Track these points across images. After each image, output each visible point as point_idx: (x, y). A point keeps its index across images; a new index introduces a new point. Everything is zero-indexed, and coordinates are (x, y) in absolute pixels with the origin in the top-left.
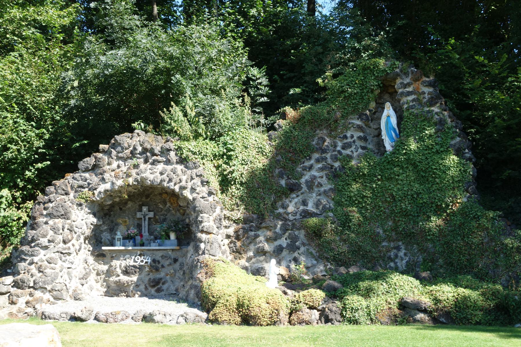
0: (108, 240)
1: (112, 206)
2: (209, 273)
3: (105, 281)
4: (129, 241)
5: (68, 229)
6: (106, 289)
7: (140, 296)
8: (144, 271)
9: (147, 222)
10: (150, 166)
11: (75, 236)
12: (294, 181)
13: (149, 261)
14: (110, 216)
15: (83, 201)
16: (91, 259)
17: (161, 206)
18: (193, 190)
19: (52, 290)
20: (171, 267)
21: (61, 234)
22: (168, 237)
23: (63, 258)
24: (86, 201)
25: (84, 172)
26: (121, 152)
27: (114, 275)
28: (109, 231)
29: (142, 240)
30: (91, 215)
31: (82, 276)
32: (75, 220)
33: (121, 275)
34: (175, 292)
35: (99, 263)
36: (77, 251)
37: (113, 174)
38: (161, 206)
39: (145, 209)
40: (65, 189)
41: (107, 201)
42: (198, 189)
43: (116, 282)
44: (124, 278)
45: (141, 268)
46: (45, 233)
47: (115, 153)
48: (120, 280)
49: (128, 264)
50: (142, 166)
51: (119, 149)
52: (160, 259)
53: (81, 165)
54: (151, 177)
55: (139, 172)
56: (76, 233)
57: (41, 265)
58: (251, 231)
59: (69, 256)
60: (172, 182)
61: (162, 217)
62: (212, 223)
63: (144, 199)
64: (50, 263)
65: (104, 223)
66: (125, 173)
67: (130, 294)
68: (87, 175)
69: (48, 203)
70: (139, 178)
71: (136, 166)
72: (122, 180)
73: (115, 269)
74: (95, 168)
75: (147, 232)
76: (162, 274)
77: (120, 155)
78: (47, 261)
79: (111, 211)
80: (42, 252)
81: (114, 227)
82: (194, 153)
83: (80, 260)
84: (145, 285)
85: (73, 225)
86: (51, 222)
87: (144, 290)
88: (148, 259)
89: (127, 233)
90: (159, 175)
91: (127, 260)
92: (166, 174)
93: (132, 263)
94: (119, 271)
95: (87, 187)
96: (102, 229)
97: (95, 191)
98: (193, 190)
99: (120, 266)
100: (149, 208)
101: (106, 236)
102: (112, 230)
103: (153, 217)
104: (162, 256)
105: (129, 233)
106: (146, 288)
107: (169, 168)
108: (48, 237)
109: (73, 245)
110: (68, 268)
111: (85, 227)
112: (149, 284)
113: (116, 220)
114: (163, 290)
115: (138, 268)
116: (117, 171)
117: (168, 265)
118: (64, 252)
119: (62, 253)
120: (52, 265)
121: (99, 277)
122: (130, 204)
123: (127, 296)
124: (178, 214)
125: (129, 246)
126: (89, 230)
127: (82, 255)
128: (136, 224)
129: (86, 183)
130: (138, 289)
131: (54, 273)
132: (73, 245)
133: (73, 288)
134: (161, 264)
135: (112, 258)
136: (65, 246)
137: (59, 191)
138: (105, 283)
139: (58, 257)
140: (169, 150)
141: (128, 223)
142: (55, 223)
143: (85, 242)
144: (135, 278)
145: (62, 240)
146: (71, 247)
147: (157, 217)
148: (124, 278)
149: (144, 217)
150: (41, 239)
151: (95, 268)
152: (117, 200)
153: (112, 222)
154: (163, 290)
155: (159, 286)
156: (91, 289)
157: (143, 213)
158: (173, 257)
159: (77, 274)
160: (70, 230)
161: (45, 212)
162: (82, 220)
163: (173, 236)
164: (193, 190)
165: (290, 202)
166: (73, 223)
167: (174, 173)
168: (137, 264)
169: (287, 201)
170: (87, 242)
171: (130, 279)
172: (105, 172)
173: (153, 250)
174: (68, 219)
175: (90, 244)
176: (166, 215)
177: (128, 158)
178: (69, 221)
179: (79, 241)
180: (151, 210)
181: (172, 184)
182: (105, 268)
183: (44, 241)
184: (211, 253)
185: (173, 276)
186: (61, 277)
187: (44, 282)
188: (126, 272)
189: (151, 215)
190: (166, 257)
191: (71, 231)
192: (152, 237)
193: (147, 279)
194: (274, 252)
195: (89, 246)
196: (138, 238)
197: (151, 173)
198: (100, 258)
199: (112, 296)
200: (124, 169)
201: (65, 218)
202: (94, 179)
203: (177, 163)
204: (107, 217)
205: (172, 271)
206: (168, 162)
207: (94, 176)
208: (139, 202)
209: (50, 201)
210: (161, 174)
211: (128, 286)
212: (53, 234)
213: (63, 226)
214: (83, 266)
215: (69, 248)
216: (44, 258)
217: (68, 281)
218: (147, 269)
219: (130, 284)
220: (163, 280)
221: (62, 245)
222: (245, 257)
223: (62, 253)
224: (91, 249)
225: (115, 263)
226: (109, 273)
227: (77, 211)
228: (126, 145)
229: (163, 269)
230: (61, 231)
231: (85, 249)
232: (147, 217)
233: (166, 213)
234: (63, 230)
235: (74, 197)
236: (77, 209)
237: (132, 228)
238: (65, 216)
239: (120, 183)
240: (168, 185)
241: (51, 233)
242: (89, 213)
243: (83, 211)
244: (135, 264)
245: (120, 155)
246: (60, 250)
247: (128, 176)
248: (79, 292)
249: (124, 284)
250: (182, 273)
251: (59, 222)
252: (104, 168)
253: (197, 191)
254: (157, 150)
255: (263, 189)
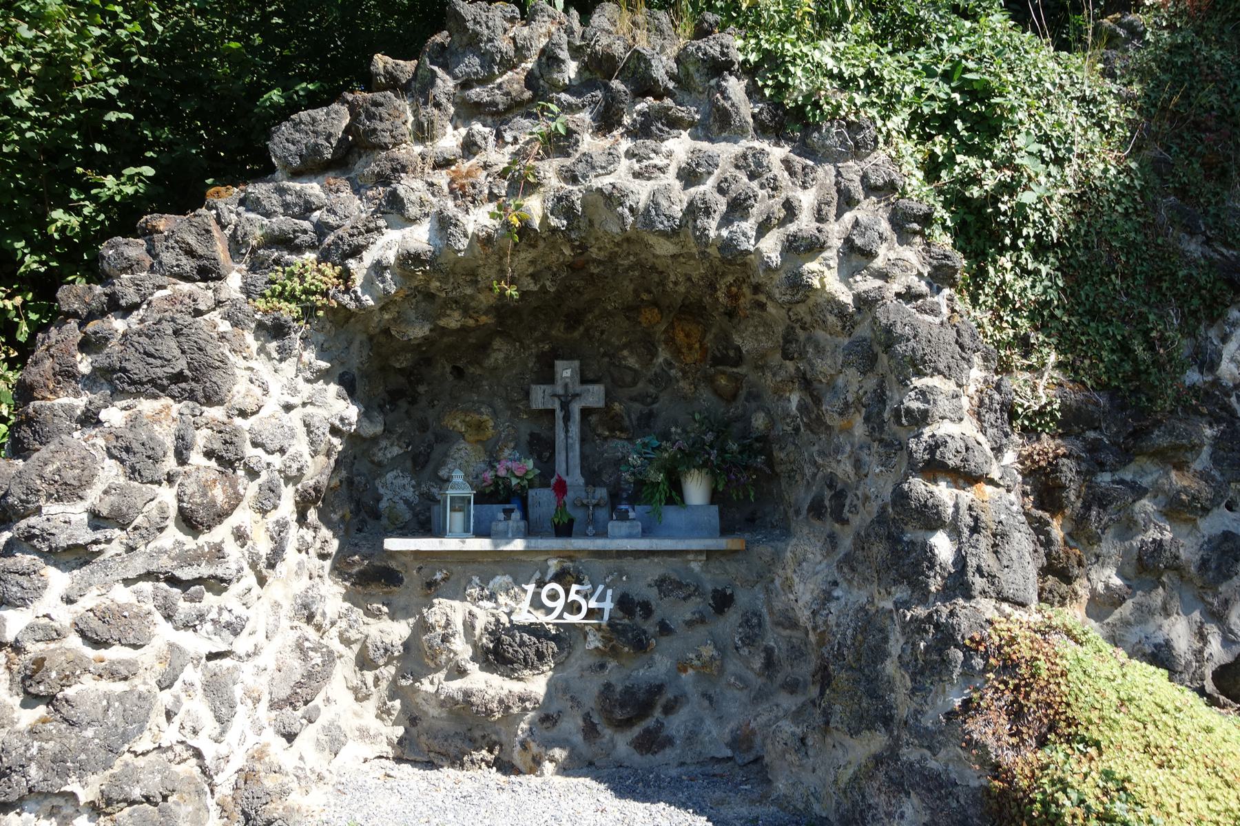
0: (407, 502)
1: (425, 353)
2: (1034, 713)
3: (395, 692)
4: (508, 513)
5: (209, 454)
6: (400, 731)
7: (565, 770)
8: (578, 653)
9: (575, 429)
10: (626, 144)
11: (251, 490)
12: (1224, 251)
13: (608, 605)
14: (413, 401)
15: (289, 311)
16: (332, 597)
17: (632, 362)
18: (856, 255)
19: (109, 802)
20: (702, 631)
21: (170, 479)
22: (675, 494)
23: (184, 608)
24: (309, 312)
25: (296, 174)
26: (482, 82)
27: (438, 669)
28: (409, 464)
29: (561, 506)
30: (333, 388)
31: (284, 692)
32: (250, 405)
33: (473, 667)
34: (729, 753)
35: (368, 613)
36: (262, 565)
37: (442, 178)
38: (632, 362)
39: (566, 371)
40: (200, 251)
41: (409, 322)
42: (884, 254)
43: (448, 702)
44: (486, 685)
45: (565, 638)
46: (70, 475)
47: (451, 83)
48: (467, 694)
49: (504, 619)
50: (588, 143)
51: (471, 64)
52: (652, 594)
53: (286, 141)
54: (641, 192)
55: (580, 168)
56: (253, 474)
57: (39, 662)
58: (1102, 466)
59: (219, 592)
60: (745, 217)
61: (637, 406)
62: (969, 428)
63: (558, 331)
64: (98, 644)
65: (388, 431)
66: (503, 174)
67: (517, 757)
68: (313, 188)
69: (103, 314)
70: (576, 193)
71: (559, 144)
72: (492, 207)
73: (445, 639)
74: (349, 155)
75: (578, 471)
76: (660, 665)
77: (477, 93)
78: (82, 634)
79: (420, 381)
80: (58, 580)
81: (430, 446)
82: (846, 83)
83: (277, 605)
84: (587, 717)
85: (236, 432)
86: (114, 416)
87: (578, 739)
88: (601, 599)
89: (489, 475)
90: (678, 185)
91: (502, 599)
92: (711, 182)
93: (525, 615)
94: (461, 648)
95: (312, 247)
96: (379, 456)
97: (352, 263)
98: (856, 255)
99: (469, 627)
100: (582, 371)
101: (396, 488)
102: (424, 461)
103: (601, 404)
104: (661, 583)
105: (502, 473)
106: (590, 731)
107: (725, 151)
108: (93, 496)
109: (240, 536)
110: (211, 657)
111: (301, 446)
112: (607, 713)
113: (239, 271)
114: (669, 741)
115: (554, 638)
116: (465, 166)
117: (690, 624)
118: (185, 574)
119: (173, 581)
120: (116, 653)
121: (369, 676)
122: (500, 352)
123: (505, 767)
124: (705, 394)
125: (506, 536)
126: (321, 459)
127: (285, 591)
128: (525, 438)
129: (306, 225)
130: (554, 732)
131: (121, 698)
132: (240, 536)
133: (238, 761)
134: (656, 617)
135: (431, 589)
136: (190, 543)
137: (168, 258)
138: (397, 703)
139: (149, 606)
140: (719, 67)
141: (490, 432)
142: (134, 423)
143: (302, 519)
144: (536, 685)
145: (173, 512)
146: (232, 549)
147: (617, 406)
148: (486, 685)
149: (565, 406)
150: (51, 508)
151: (353, 634)
152: (453, 320)
153: (423, 427)
154: (669, 741)
155: (649, 722)
156: (334, 743)
157: (559, 390)
158: (709, 587)
159: (261, 685)
160: (220, 459)
161: (84, 365)
162: (288, 408)
163: (696, 490)
164: (856, 260)
165: (1225, 339)
166: (238, 421)
167: (752, 177)
168: (551, 618)
169: (1213, 333)
170: (312, 515)
171: (517, 687)
172: (404, 169)
173: (621, 554)
174: (209, 401)
175: (329, 525)
176: (656, 399)
177: (517, 107)
178: (215, 413)
179: (273, 516)
180: (591, 376)
181: (749, 226)
182: (398, 631)
183: (66, 519)
184: (1009, 591)
185: (710, 672)
186: (169, 715)
187: (59, 764)
188: (497, 655)
189: (594, 396)
190: (680, 585)
191: (226, 463)
192: (602, 493)
193: (591, 688)
194: (1204, 565)
195: (325, 533)
196: (542, 499)
197: (637, 175)
198: (374, 589)
199: (430, 765)
200: (500, 158)
201: (192, 397)
202: (347, 205)
203: (762, 129)
204: (403, 405)
205: (708, 651)
206: (718, 123)
207: (346, 194)
208: (537, 341)
209: (115, 306)
210: (689, 176)
211: (509, 719)
212: (122, 480)
213: (180, 437)
214: (293, 636)
215: (218, 553)
216: (64, 616)
217: (209, 725)
218: (594, 642)
219: (515, 710)
220: (669, 694)
221: (173, 536)
222: (1084, 594)
223: (173, 581)
224: (334, 546)
225: (449, 611)
226: (417, 656)
227: (262, 367)
228: (504, 45)
229: (665, 641)
230: (170, 463)
231: (303, 548)
232: (576, 408)
233: (652, 390)
234: (182, 460)
235: (247, 290)
236: (261, 350)
237: (507, 452)
238: (195, 382)
239: (479, 219)
240: (725, 233)
241: (110, 472)
242: (324, 375)
243: (289, 367)
244: (539, 617)
245: (477, 93)
246: (164, 564)
247: (522, 184)
248: (270, 782)
249: (490, 713)
250: (757, 663)
251: (160, 416)
252: (401, 153)
253: (878, 263)
254: (662, 68)
255: (1123, 277)
